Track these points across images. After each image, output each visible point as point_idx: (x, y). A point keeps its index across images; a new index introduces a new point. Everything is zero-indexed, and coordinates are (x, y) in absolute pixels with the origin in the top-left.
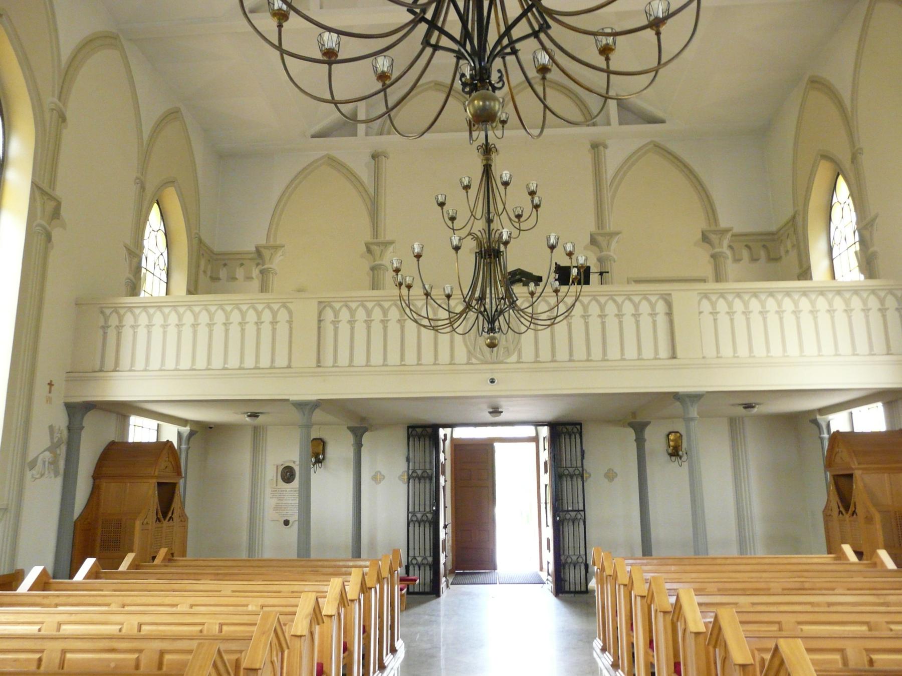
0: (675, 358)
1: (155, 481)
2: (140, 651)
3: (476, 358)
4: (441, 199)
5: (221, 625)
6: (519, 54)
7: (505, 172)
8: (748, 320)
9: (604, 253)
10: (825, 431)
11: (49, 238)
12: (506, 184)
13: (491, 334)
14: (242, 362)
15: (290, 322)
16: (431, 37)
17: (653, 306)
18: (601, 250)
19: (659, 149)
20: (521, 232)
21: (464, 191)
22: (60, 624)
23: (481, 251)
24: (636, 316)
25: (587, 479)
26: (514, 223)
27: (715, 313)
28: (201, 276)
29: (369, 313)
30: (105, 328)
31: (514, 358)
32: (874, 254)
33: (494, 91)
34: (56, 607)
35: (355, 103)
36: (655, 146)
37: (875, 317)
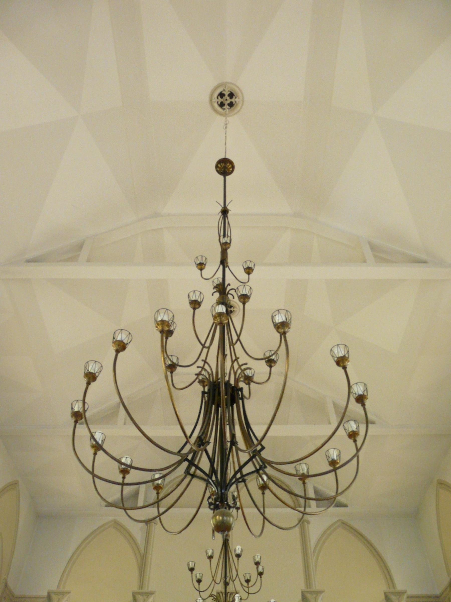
4: (191, 565)
6: (247, 482)
7: (238, 547)
12: (238, 556)
16: (190, 470)
19: (345, 525)
20: (250, 595)
21: (208, 560)
26: (245, 588)
33: (229, 509)
35: (138, 486)
36: (342, 523)
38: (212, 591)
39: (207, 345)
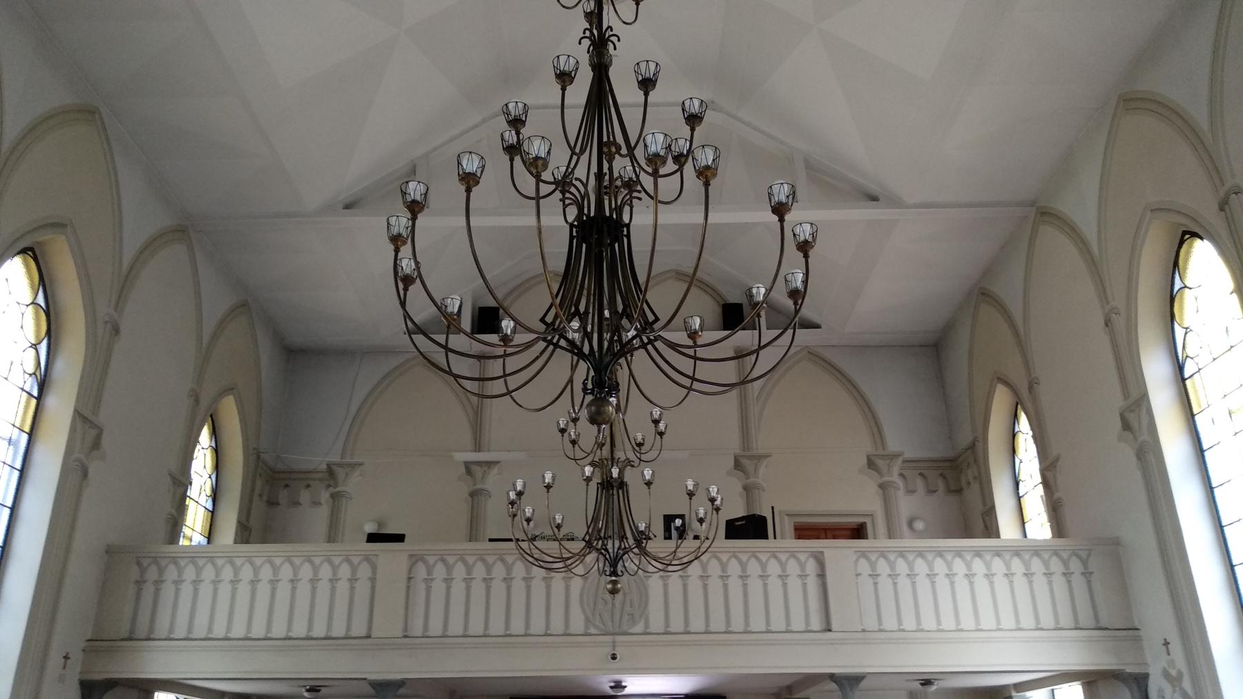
0: (830, 630)
3: (596, 627)
9: (751, 480)
11: (85, 474)
13: (614, 578)
14: (310, 629)
15: (373, 580)
18: (747, 475)
20: (642, 462)
23: (604, 482)
24: (783, 577)
28: (256, 498)
29: (469, 570)
30: (140, 583)
31: (639, 628)
37: (1059, 582)
39: (577, 150)
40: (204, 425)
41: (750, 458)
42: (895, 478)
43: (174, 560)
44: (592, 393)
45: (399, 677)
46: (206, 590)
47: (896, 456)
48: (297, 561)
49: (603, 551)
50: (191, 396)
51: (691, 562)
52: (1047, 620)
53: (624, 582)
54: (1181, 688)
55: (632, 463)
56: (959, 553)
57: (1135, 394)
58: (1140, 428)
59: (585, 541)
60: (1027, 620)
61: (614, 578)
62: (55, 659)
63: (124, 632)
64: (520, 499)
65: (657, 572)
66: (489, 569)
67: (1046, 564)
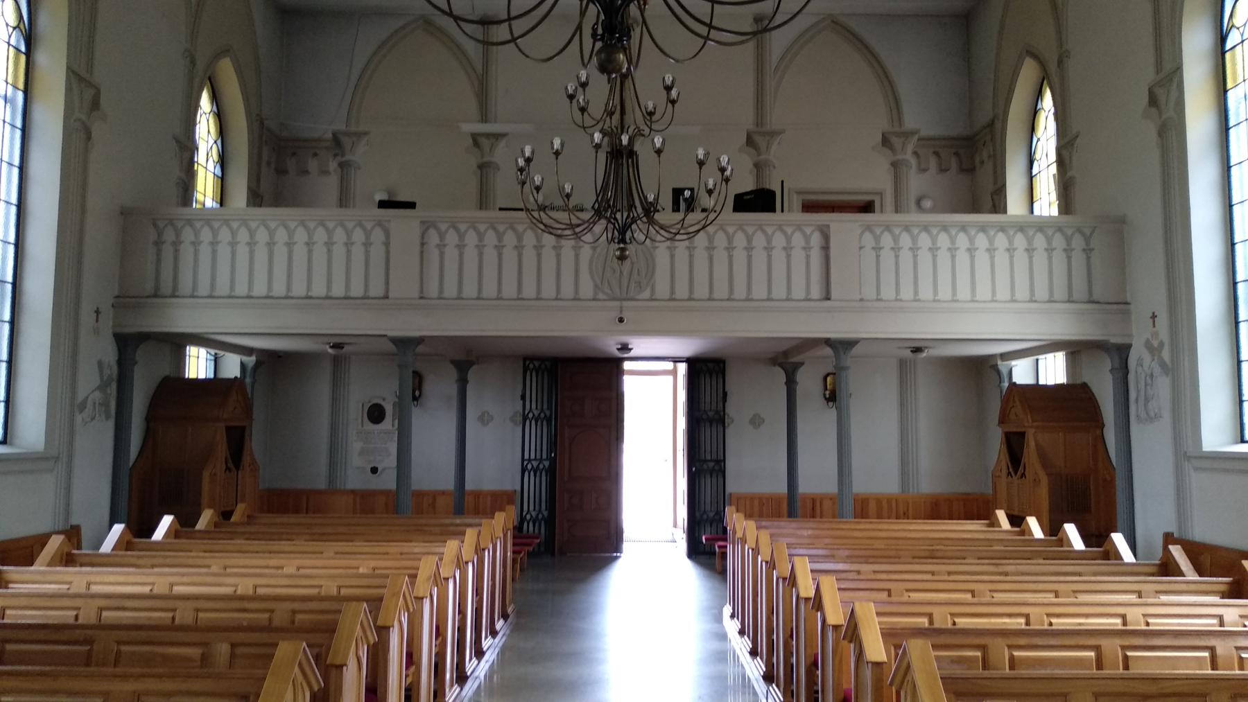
0: (829, 299)
1: (222, 425)
2: (272, 611)
3: (604, 293)
5: (339, 587)
8: (915, 257)
9: (762, 157)
10: (1006, 380)
13: (622, 245)
14: (329, 288)
15: (387, 244)
17: (807, 239)
22: (172, 585)
24: (788, 249)
25: (729, 425)
26: (648, 122)
27: (878, 248)
28: (264, 169)
29: (481, 236)
30: (158, 244)
31: (646, 294)
32: (1072, 178)
34: (153, 568)
36: (833, 22)
37: (1059, 258)
38: (589, 114)
40: (203, 90)
41: (764, 134)
42: (909, 156)
43: (189, 222)
44: (602, 39)
45: (417, 334)
46: (224, 252)
47: (907, 135)
48: (312, 225)
49: (611, 220)
50: (187, 57)
51: (698, 231)
52: (1042, 292)
53: (631, 250)
54: (1161, 358)
55: (642, 132)
56: (963, 228)
57: (1168, 67)
58: (1167, 101)
59: (594, 209)
60: (1022, 292)
61: (622, 245)
62: (87, 317)
63: (149, 287)
64: (529, 166)
65: (664, 241)
66: (500, 237)
67: (1049, 240)
